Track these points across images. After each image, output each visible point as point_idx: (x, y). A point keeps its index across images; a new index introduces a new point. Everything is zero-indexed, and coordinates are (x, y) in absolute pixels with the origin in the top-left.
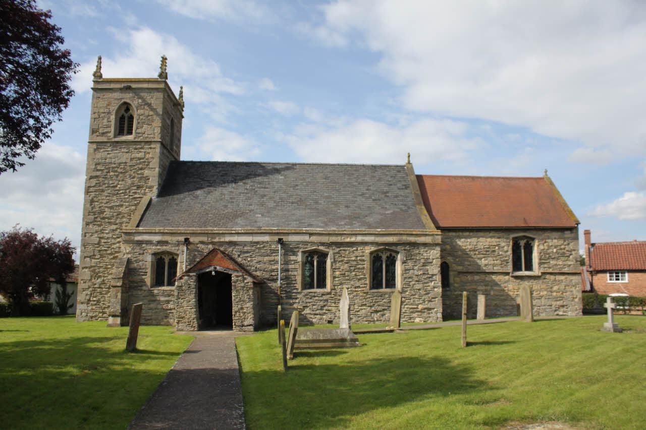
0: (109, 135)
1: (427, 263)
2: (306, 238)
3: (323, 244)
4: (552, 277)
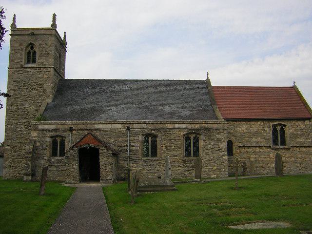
0: (21, 63)
1: (219, 141)
2: (144, 126)
3: (154, 129)
4: (298, 149)
